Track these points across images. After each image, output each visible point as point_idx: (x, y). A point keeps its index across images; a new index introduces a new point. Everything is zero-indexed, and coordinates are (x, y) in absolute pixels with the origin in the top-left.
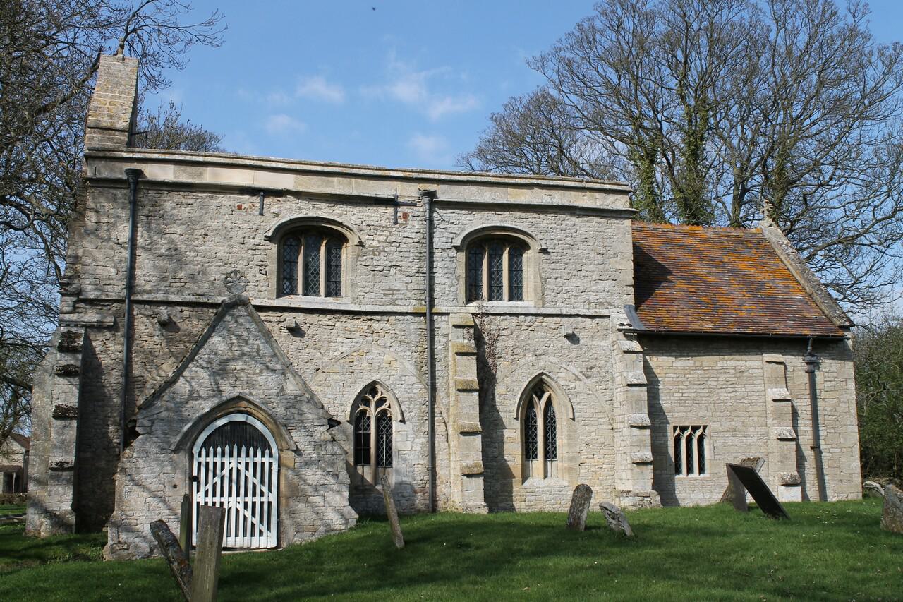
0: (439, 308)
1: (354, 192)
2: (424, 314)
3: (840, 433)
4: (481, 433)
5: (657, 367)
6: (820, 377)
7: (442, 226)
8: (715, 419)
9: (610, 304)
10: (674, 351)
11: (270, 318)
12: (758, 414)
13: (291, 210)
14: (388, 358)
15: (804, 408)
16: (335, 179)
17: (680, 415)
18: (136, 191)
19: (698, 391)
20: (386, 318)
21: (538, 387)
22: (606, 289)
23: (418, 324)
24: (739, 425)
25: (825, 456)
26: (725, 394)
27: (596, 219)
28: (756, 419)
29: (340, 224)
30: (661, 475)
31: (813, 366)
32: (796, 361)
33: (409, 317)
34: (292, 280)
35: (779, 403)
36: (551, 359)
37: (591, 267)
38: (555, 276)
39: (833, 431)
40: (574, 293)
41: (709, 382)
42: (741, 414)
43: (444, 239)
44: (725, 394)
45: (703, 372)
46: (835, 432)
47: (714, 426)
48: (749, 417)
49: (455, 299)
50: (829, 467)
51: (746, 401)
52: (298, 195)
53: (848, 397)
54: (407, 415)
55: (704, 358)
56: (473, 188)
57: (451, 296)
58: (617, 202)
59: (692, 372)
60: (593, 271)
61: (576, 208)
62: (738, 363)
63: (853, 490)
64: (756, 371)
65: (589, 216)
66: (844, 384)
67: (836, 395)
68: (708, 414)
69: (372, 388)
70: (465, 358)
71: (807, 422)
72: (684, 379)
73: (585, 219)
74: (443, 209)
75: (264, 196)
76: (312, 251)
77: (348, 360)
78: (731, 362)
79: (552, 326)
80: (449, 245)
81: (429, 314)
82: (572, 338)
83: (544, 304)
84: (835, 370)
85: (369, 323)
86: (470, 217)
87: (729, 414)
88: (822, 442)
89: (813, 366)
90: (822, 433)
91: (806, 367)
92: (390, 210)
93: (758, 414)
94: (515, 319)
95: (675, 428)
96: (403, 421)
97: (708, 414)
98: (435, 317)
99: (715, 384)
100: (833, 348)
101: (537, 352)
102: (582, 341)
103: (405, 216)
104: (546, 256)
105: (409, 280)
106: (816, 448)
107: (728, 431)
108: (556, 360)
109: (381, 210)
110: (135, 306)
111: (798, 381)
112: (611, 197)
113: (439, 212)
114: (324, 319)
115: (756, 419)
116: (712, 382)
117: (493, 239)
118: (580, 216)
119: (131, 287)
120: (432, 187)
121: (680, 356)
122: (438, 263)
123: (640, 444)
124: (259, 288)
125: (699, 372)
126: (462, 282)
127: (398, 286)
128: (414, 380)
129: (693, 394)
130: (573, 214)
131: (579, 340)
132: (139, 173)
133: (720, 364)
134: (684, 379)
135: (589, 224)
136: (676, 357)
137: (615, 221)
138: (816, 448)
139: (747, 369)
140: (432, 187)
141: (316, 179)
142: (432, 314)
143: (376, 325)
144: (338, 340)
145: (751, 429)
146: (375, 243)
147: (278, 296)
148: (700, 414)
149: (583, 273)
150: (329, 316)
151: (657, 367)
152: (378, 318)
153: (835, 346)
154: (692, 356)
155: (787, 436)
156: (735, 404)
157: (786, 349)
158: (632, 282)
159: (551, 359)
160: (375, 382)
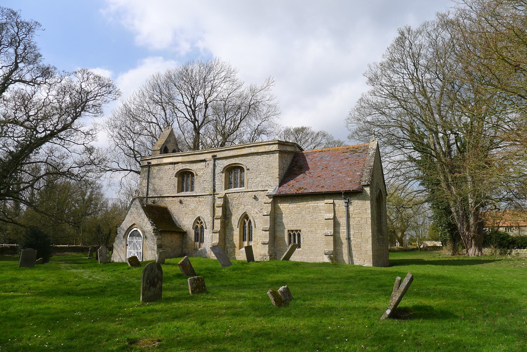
0: (217, 192)
1: (196, 159)
2: (212, 195)
3: (361, 233)
4: (219, 232)
5: (283, 208)
6: (351, 208)
7: (302, 142)
8: (304, 227)
9: (270, 185)
10: (289, 201)
11: (175, 199)
12: (322, 225)
13: (180, 167)
14: (203, 209)
15: (343, 222)
16: (191, 156)
17: (290, 226)
18: (149, 168)
19: (298, 216)
20: (203, 197)
21: (245, 216)
22: (269, 180)
23: (210, 198)
24: (313, 229)
25: (352, 243)
26: (309, 217)
27: (266, 155)
28: (321, 227)
29: (191, 170)
30: (283, 248)
31: (348, 204)
32: (341, 202)
33: (209, 196)
34: (183, 187)
35: (327, 220)
36: (249, 207)
37: (264, 173)
38: (251, 178)
39: (358, 232)
40: (258, 183)
41: (302, 213)
42: (315, 225)
43: (218, 170)
44: (309, 217)
45: (300, 209)
46: (359, 232)
47: (303, 230)
48: (318, 226)
49: (222, 189)
50: (355, 247)
51: (317, 220)
52: (182, 162)
53: (366, 216)
54: (207, 226)
55: (301, 203)
56: (227, 152)
57: (220, 188)
58: (273, 148)
59: (296, 209)
60: (264, 174)
61: (258, 153)
62: (314, 204)
63: (367, 258)
64: (322, 207)
65: (263, 155)
66: (365, 210)
67: (360, 216)
68: (301, 225)
69: (199, 218)
70: (219, 208)
71: (344, 228)
72: (293, 212)
73: (262, 156)
74: (219, 160)
75: (175, 164)
76: (188, 177)
77: (193, 210)
78: (312, 204)
79: (250, 195)
80: (220, 172)
81: (214, 193)
82: (255, 198)
83: (248, 188)
84: (360, 205)
85: (199, 199)
86: (226, 162)
87: (309, 225)
88: (352, 236)
89: (348, 204)
90: (352, 232)
91: (345, 204)
92: (204, 163)
93: (322, 225)
94: (238, 194)
95: (288, 231)
96: (206, 229)
97: (301, 225)
98: (216, 195)
99: (305, 213)
100: (360, 195)
101: (245, 205)
102: (260, 200)
103: (208, 164)
104: (248, 171)
105: (209, 184)
106: (349, 239)
107: (309, 232)
108: (250, 207)
109: (202, 163)
110: (148, 199)
111: (341, 210)
112: (271, 146)
113: (217, 161)
114: (188, 198)
115: (321, 227)
116: (303, 213)
117: (235, 168)
118: (260, 155)
119: (147, 194)
120: (215, 154)
121: (291, 203)
122: (217, 178)
123: (327, 244)
124: (173, 191)
125: (298, 209)
126: (224, 183)
127: (206, 187)
128: (209, 216)
129: (296, 218)
130: (258, 155)
131: (258, 199)
132: (149, 163)
133: (306, 205)
134: (293, 212)
135: (263, 158)
136: (290, 203)
137: (272, 155)
138: (349, 239)
139: (318, 207)
140: (215, 154)
141: (186, 157)
142: (214, 195)
143: (201, 199)
144: (191, 204)
145: (319, 231)
146: (200, 174)
147: (178, 192)
148: (298, 225)
149: (261, 175)
150: (189, 198)
151: (283, 208)
152: (201, 197)
153: (360, 194)
154: (296, 203)
155: (328, 234)
156: (312, 221)
157: (336, 197)
158: (278, 176)
159: (249, 207)
160: (199, 217)
